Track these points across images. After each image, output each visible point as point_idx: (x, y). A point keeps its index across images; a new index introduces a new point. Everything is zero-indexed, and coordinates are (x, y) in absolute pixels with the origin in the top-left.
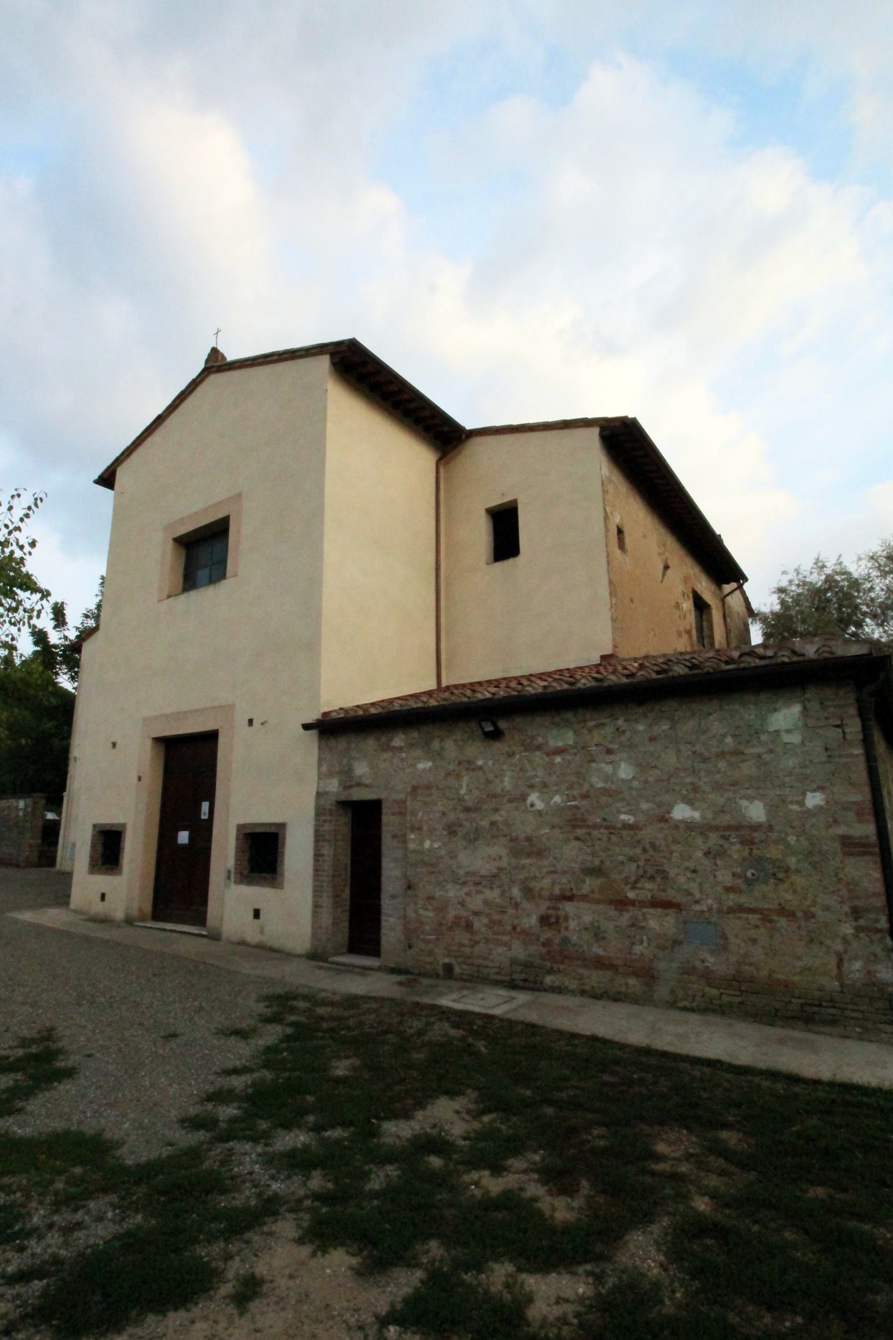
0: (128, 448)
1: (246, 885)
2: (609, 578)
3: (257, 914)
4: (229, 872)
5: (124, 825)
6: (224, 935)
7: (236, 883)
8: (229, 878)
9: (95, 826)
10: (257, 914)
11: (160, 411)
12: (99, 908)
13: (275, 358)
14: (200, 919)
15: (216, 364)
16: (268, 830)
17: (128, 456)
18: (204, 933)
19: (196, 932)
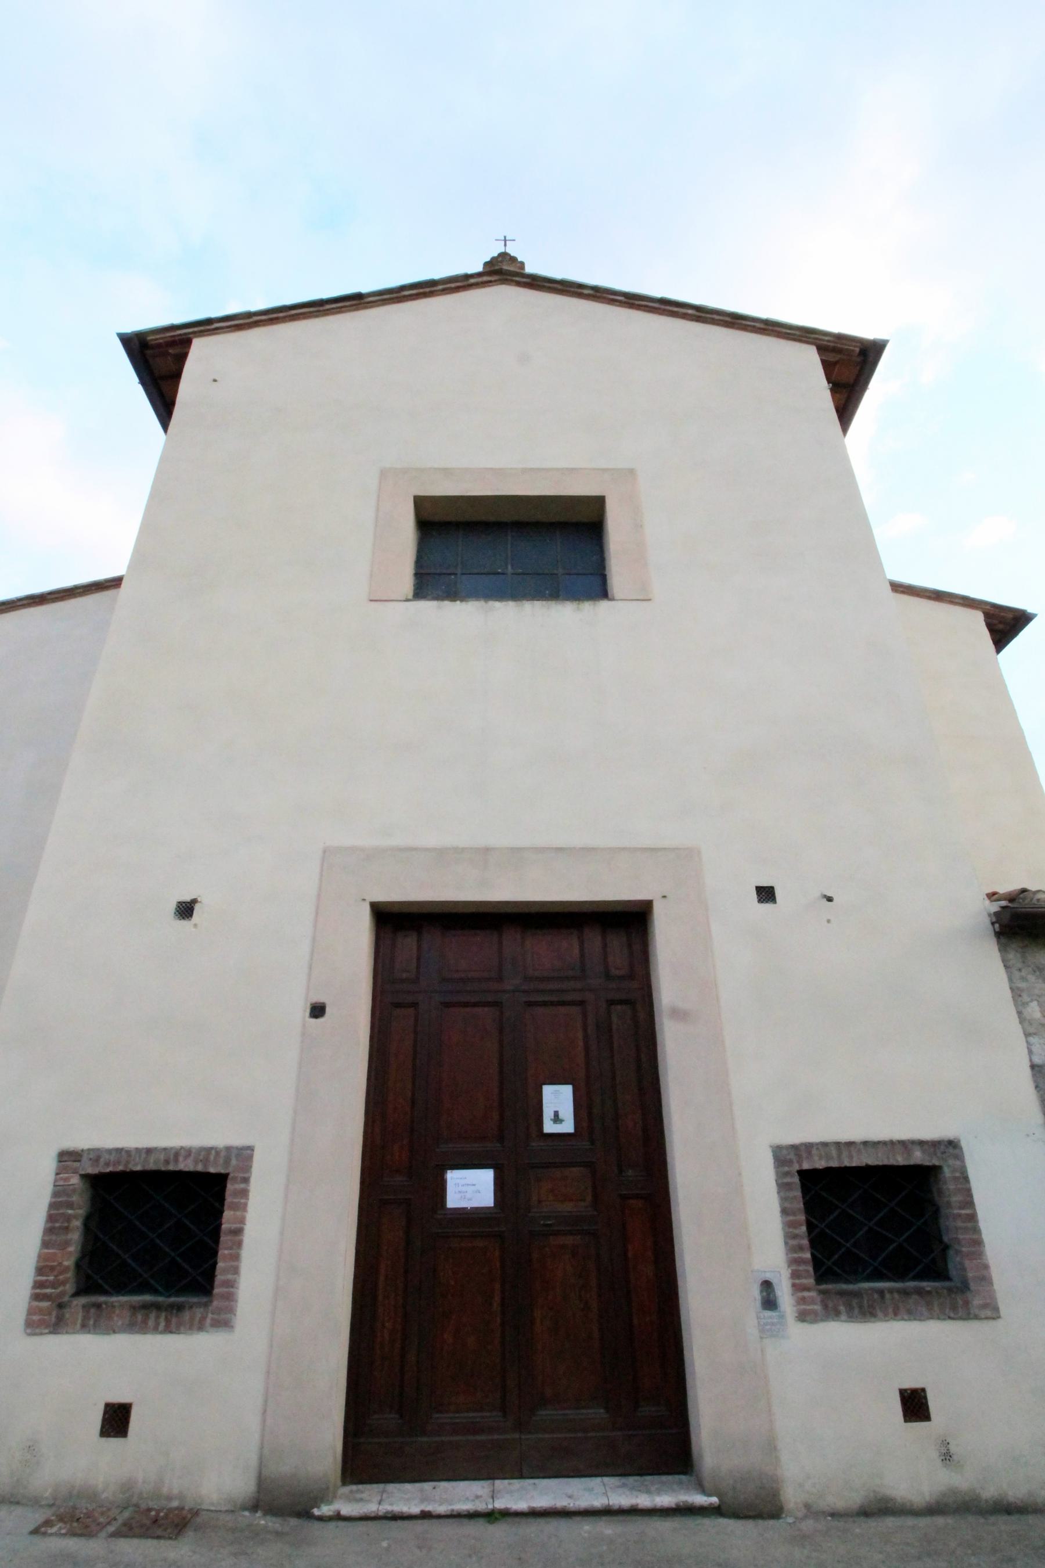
0: (249, 315)
1: (851, 1318)
2: (493, 849)
3: (914, 1405)
4: (767, 1285)
5: (245, 1155)
6: (792, 1497)
7: (803, 1317)
8: (769, 1303)
9: (67, 1158)
10: (914, 1405)
11: (365, 289)
12: (102, 1467)
13: (586, 292)
14: (666, 1446)
15: (503, 271)
16: (900, 1160)
17: (239, 328)
18: (699, 1499)
19: (665, 1500)
